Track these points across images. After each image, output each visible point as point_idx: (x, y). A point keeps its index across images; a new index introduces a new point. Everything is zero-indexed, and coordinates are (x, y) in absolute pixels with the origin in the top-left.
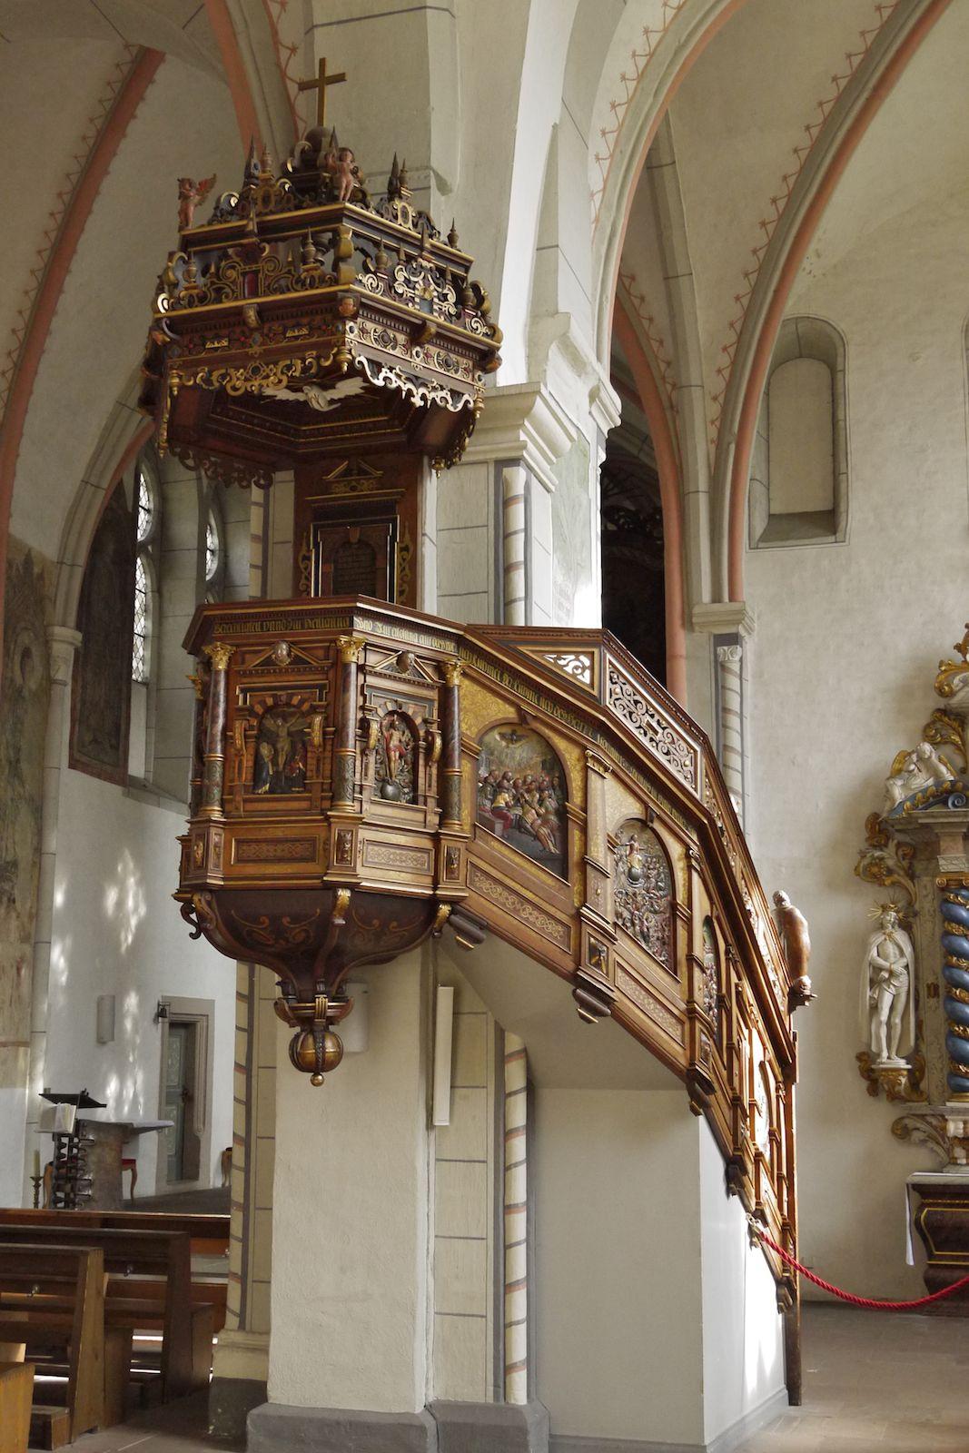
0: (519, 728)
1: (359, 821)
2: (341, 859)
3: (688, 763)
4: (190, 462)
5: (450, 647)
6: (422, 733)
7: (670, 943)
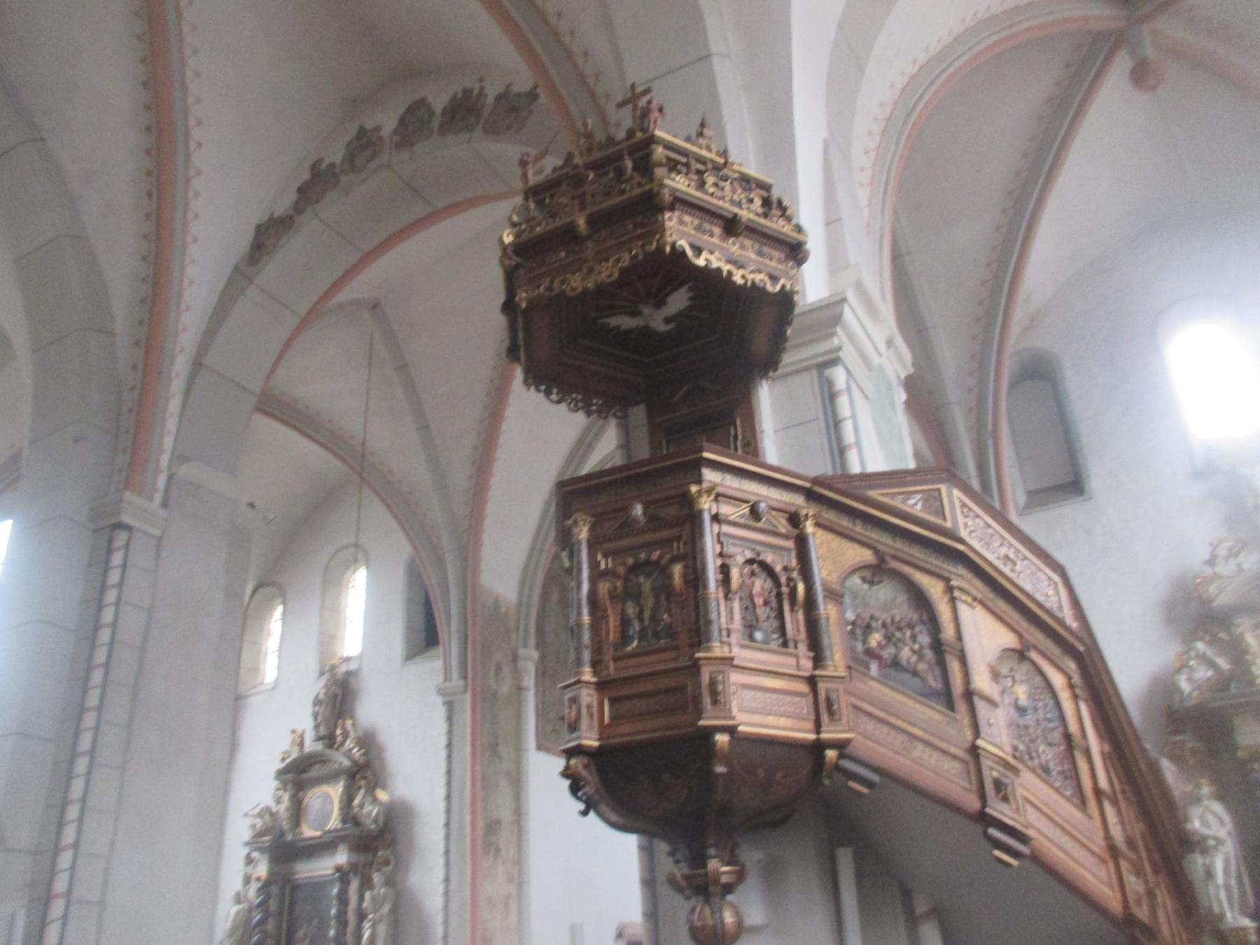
0: (878, 571)
1: (728, 661)
2: (715, 702)
3: (1051, 592)
4: (554, 397)
5: (798, 500)
6: (783, 580)
7: (1074, 776)
